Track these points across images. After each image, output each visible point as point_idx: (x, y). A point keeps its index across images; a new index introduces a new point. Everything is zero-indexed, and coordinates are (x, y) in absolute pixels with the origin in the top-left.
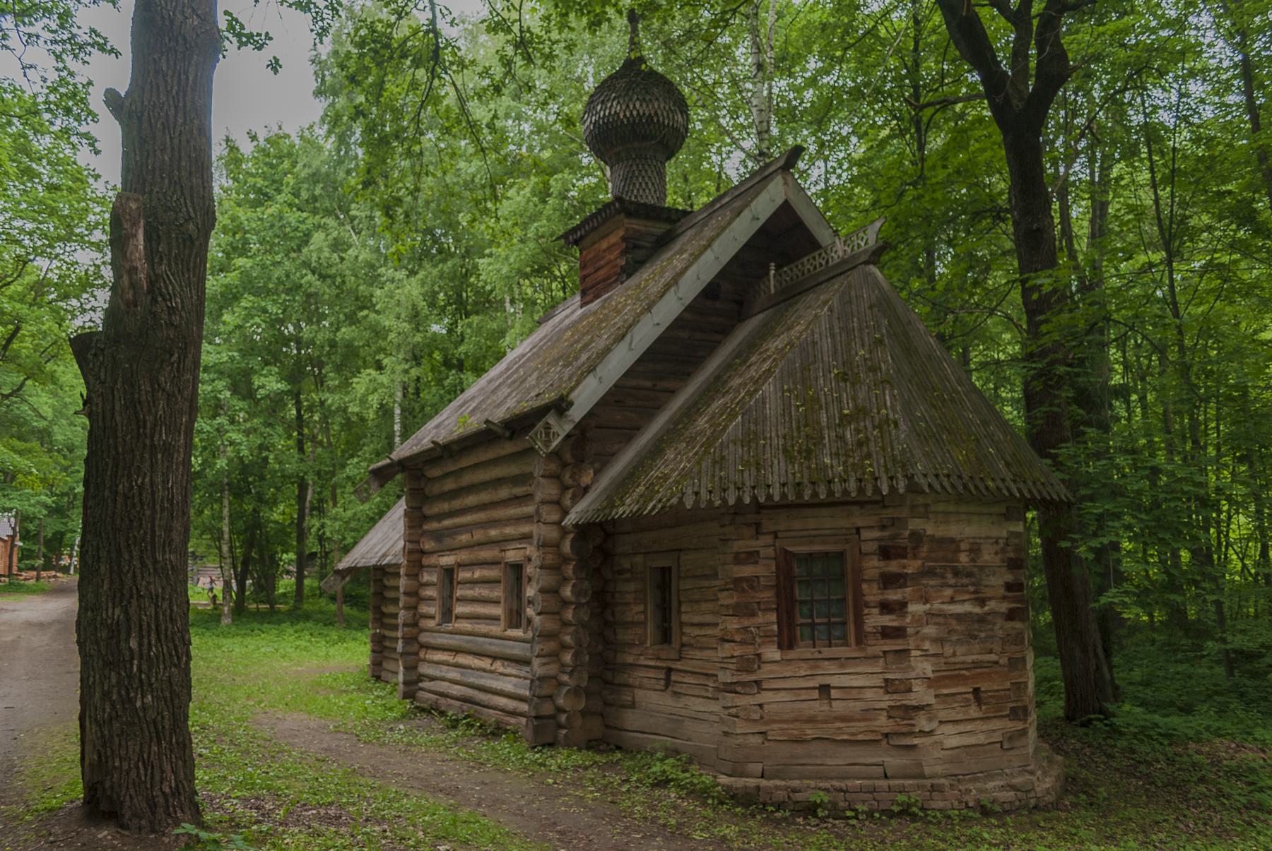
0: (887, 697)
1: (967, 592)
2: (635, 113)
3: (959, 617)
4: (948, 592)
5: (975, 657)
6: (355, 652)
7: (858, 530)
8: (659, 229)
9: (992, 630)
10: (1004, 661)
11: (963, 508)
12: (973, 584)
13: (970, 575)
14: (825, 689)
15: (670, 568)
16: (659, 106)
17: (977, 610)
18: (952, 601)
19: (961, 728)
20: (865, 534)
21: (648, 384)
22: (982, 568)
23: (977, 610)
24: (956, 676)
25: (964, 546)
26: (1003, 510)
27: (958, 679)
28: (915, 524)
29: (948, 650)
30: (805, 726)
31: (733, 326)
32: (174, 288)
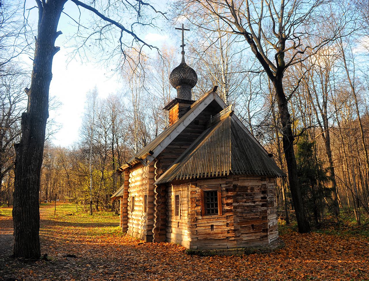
0: (227, 228)
1: (250, 200)
2: (182, 77)
3: (248, 206)
4: (245, 200)
5: (252, 217)
7: (221, 185)
8: (187, 106)
9: (257, 209)
10: (261, 217)
11: (249, 178)
12: (252, 198)
13: (251, 195)
14: (212, 226)
15: (178, 196)
16: (188, 76)
17: (253, 204)
18: (245, 202)
19: (248, 235)
20: (222, 186)
21: (179, 147)
22: (254, 194)
23: (253, 204)
24: (247, 222)
25: (249, 188)
26: (260, 178)
27: (247, 222)
28: (235, 183)
29: (244, 215)
30: (208, 236)
31: (203, 131)
32: (36, 133)
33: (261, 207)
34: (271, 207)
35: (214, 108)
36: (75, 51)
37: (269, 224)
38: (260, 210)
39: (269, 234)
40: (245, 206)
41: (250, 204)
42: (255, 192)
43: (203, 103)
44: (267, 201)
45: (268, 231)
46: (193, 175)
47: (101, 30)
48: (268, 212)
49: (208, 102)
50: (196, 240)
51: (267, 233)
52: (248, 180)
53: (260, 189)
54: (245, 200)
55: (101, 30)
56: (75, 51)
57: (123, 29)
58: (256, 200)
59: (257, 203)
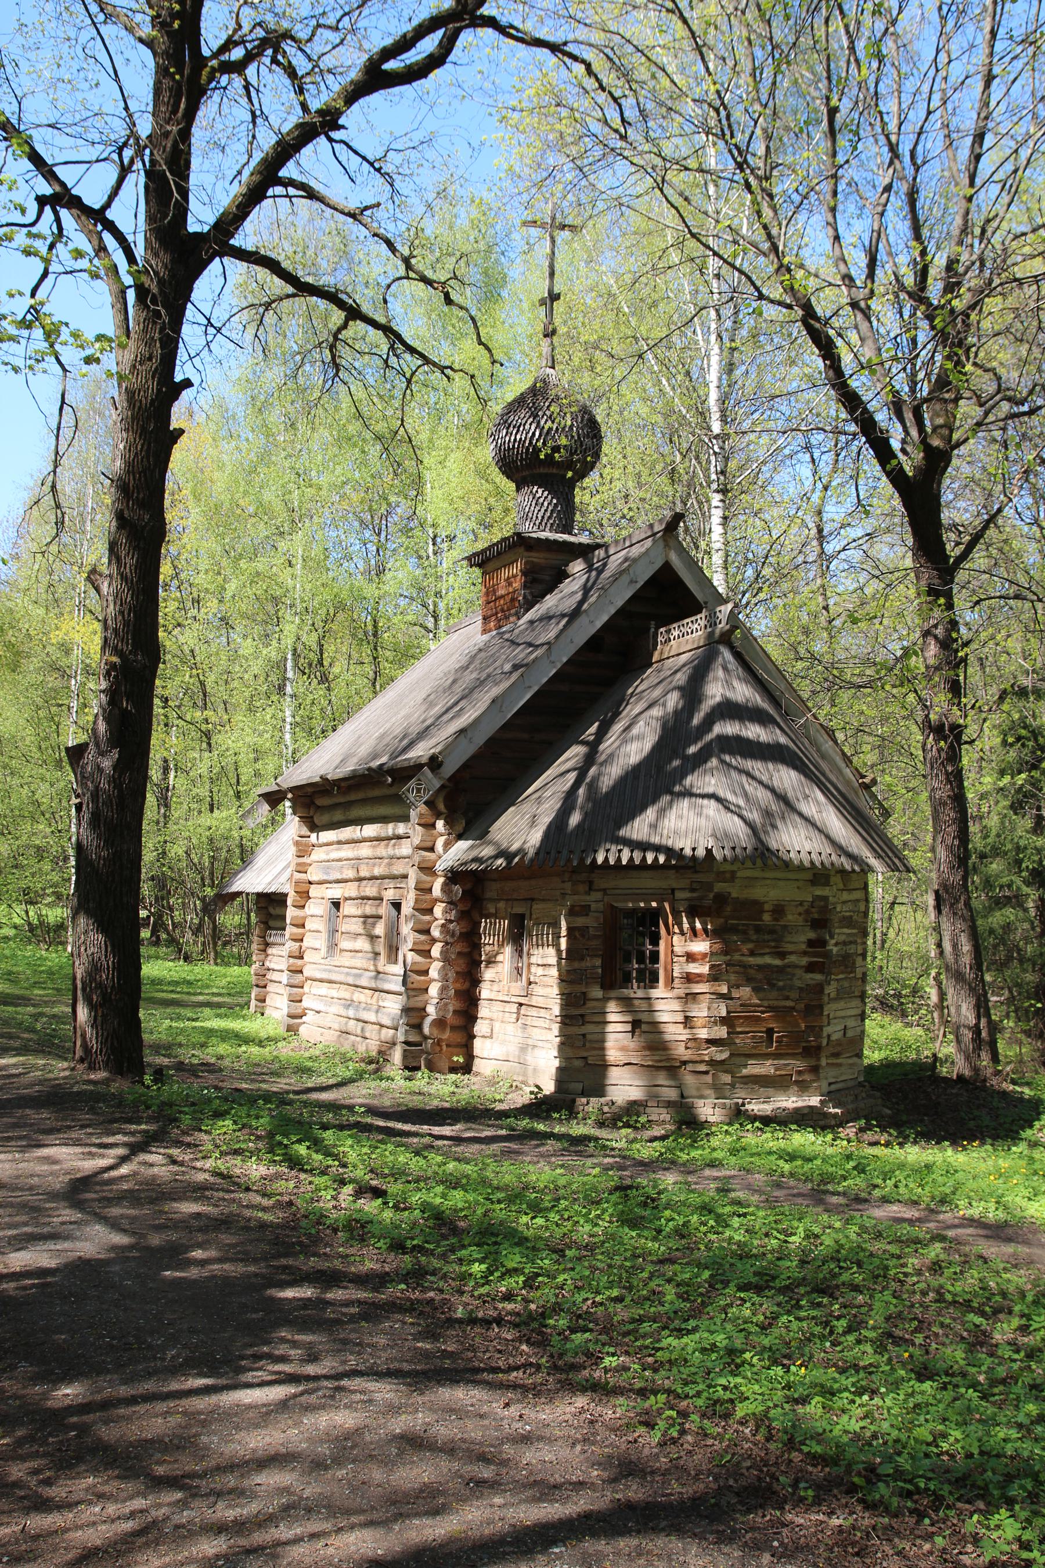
6: (549, 1087)
7: (673, 890)
17: (777, 962)
18: (752, 953)
20: (679, 895)
22: (785, 927)
23: (777, 962)
25: (767, 907)
35: (669, 594)
38: (798, 983)
41: (768, 960)
43: (625, 579)
44: (827, 955)
49: (644, 574)
50: (578, 1063)
58: (790, 948)
59: (793, 958)
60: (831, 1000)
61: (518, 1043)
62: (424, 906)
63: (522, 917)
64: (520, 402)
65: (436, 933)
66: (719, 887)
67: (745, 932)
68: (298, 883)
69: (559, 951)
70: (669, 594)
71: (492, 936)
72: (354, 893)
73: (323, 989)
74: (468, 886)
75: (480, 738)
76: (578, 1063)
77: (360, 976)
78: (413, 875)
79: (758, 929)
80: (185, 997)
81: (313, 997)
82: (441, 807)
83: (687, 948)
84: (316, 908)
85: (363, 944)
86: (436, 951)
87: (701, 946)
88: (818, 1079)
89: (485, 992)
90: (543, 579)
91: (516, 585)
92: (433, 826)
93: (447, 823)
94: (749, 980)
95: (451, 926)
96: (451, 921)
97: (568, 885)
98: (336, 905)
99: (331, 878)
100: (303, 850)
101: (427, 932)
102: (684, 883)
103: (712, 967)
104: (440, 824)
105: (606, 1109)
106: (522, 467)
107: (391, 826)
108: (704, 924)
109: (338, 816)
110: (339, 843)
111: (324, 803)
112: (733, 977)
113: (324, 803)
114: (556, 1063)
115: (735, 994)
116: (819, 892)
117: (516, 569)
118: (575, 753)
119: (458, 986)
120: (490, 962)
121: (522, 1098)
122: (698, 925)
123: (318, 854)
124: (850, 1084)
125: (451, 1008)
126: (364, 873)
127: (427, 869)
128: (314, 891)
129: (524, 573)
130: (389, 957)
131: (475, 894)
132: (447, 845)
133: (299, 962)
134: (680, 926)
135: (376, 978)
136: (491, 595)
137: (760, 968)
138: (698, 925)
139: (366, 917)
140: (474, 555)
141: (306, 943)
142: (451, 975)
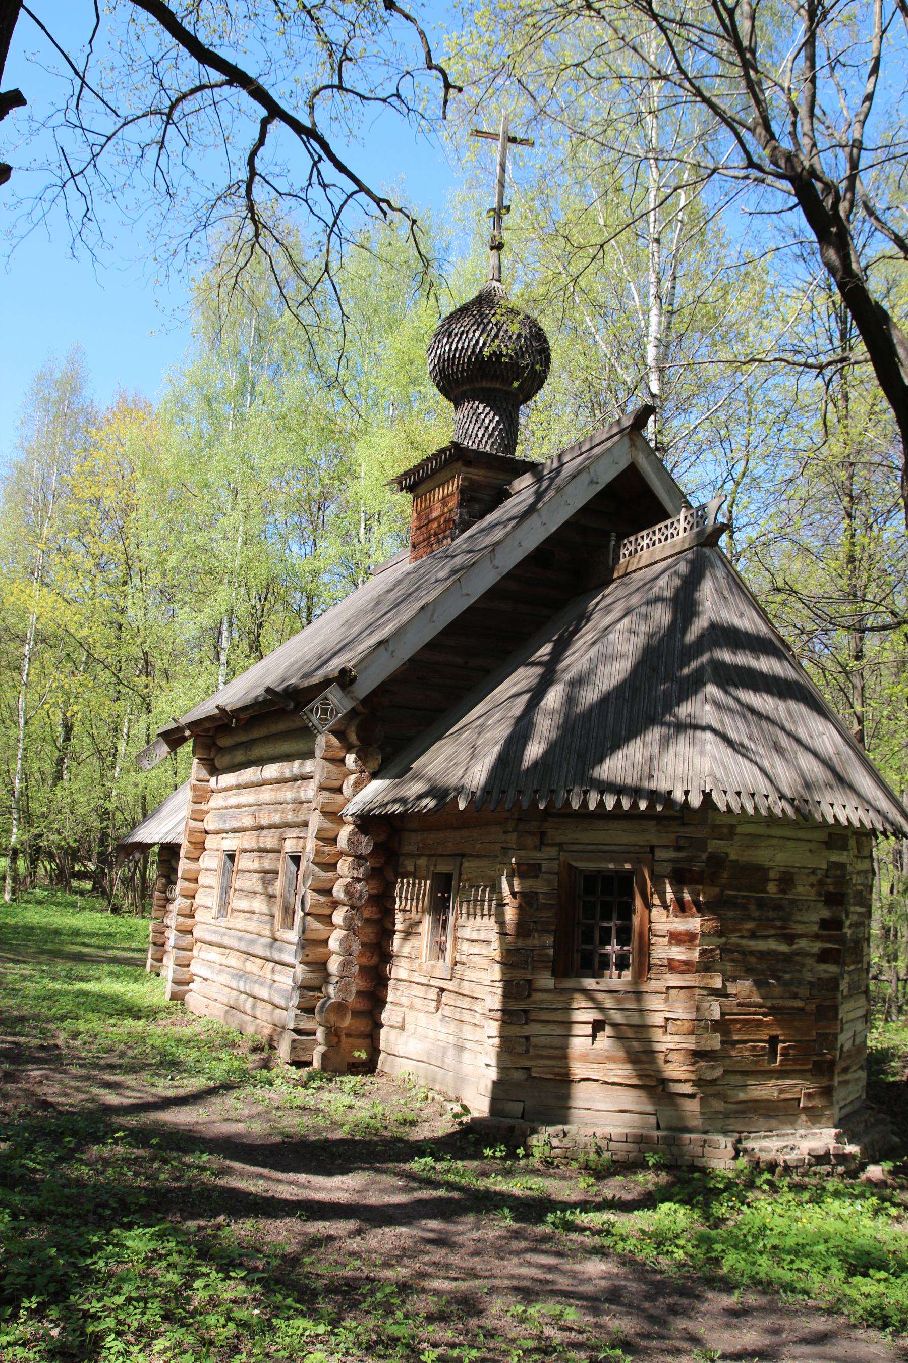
1: (774, 927)
4: (750, 925)
6: (480, 1107)
7: (652, 848)
12: (781, 919)
17: (784, 948)
18: (753, 936)
20: (660, 854)
22: (793, 902)
23: (784, 948)
25: (772, 875)
33: (818, 962)
34: (852, 967)
35: (632, 499)
36: (50, 195)
37: (842, 1038)
38: (808, 977)
39: (836, 1084)
40: (752, 953)
41: (772, 945)
42: (799, 894)
43: (584, 478)
44: (841, 940)
45: (836, 1072)
46: (536, 791)
47: (173, 107)
48: (844, 986)
49: (607, 474)
50: (518, 1076)
51: (832, 1079)
52: (775, 841)
53: (821, 883)
54: (750, 925)
55: (173, 107)
56: (50, 195)
57: (275, 111)
58: (799, 929)
59: (803, 943)
60: (844, 997)
61: (443, 1041)
62: (326, 860)
63: (448, 877)
64: (463, 311)
65: (338, 891)
66: (714, 845)
67: (745, 907)
68: (192, 832)
69: (501, 923)
70: (632, 499)
71: (408, 903)
72: (253, 845)
73: (213, 954)
74: (382, 838)
75: (406, 651)
76: (518, 1076)
77: (252, 942)
78: (316, 821)
79: (761, 904)
80: (102, 953)
81: (204, 961)
82: (353, 738)
83: (669, 925)
84: (211, 861)
85: (259, 904)
86: (338, 917)
87: (694, 924)
88: (831, 1105)
89: (399, 971)
90: (481, 499)
91: (452, 504)
92: (342, 761)
93: (359, 757)
94: (749, 971)
95: (358, 886)
96: (358, 880)
97: (512, 837)
98: (231, 857)
99: (227, 827)
100: (201, 796)
101: (329, 892)
102: (668, 838)
103: (703, 952)
104: (350, 759)
105: (555, 1142)
106: (463, 379)
107: (297, 763)
108: (695, 894)
109: (239, 757)
110: (239, 787)
111: (223, 740)
112: (729, 967)
113: (223, 740)
114: (493, 1074)
115: (732, 989)
116: (836, 857)
117: (452, 487)
118: (522, 678)
119: (364, 961)
120: (408, 934)
121: (443, 1127)
122: (687, 896)
123: (216, 801)
124: (857, 1105)
125: (354, 989)
126: (264, 822)
127: (333, 815)
128: (210, 842)
129: (462, 491)
130: (284, 920)
131: (388, 842)
132: (358, 786)
133: (189, 921)
134: (662, 894)
135: (271, 946)
136: (423, 521)
137: (763, 955)
138: (687, 896)
139: (267, 872)
140: (407, 474)
141: (198, 900)
142: (356, 947)
